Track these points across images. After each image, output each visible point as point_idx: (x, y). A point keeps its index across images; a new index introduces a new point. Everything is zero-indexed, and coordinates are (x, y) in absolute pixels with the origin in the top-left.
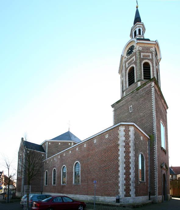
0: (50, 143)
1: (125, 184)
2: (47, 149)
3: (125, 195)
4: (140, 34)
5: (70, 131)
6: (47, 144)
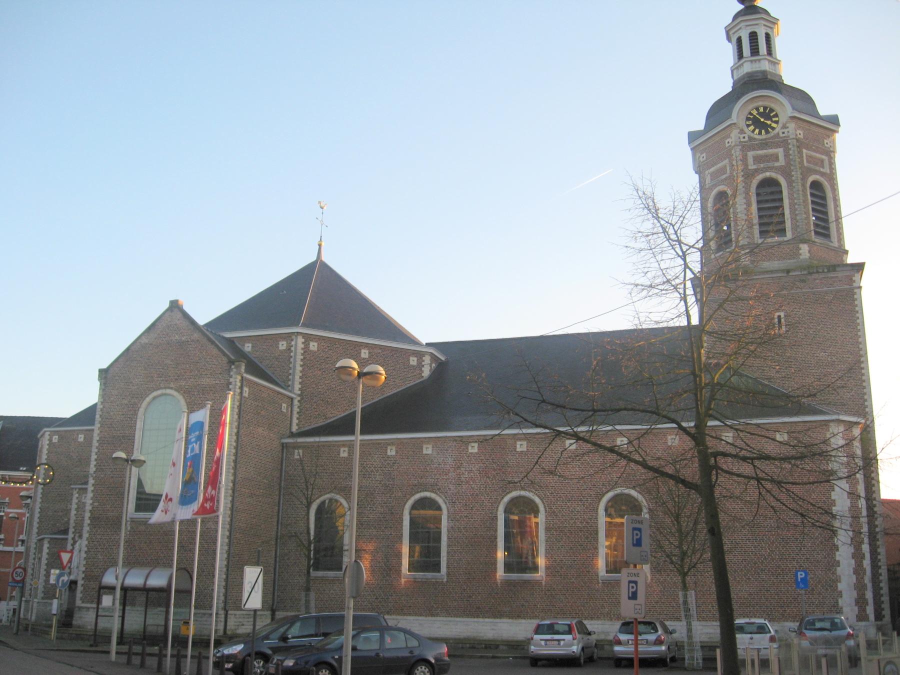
0: (313, 346)
1: (855, 584)
2: (298, 375)
3: (857, 616)
4: (755, 51)
5: (325, 258)
6: (300, 345)
